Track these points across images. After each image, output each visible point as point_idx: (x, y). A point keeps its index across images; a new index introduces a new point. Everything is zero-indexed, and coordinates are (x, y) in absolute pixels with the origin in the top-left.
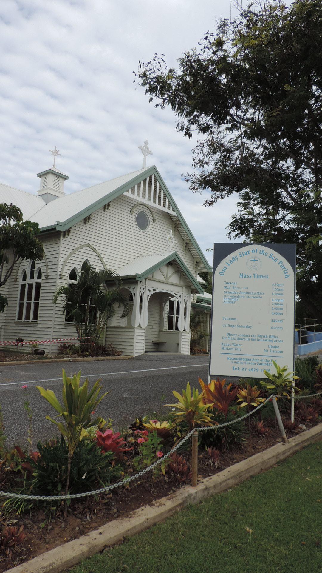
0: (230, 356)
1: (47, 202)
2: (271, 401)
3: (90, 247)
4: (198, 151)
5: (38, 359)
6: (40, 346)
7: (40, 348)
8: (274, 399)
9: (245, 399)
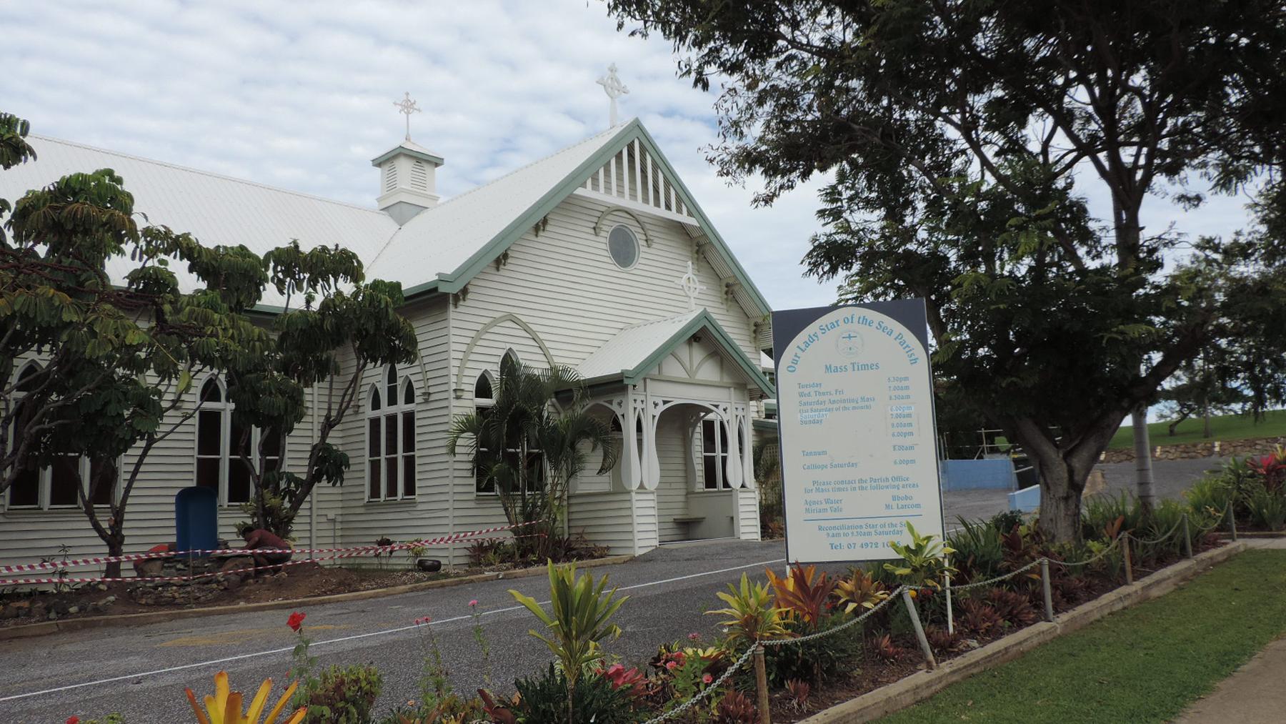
0: (823, 524)
1: (401, 222)
2: (900, 596)
3: (513, 319)
4: (726, 105)
5: (430, 579)
6: (429, 553)
7: (430, 555)
8: (909, 594)
9: (852, 597)
